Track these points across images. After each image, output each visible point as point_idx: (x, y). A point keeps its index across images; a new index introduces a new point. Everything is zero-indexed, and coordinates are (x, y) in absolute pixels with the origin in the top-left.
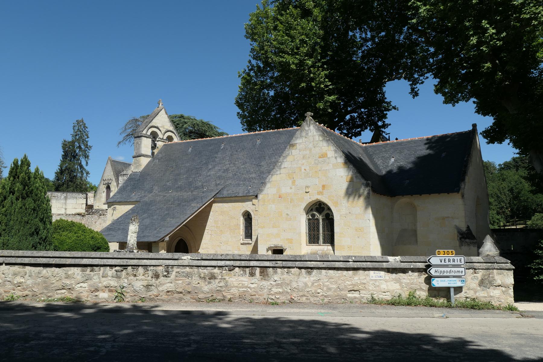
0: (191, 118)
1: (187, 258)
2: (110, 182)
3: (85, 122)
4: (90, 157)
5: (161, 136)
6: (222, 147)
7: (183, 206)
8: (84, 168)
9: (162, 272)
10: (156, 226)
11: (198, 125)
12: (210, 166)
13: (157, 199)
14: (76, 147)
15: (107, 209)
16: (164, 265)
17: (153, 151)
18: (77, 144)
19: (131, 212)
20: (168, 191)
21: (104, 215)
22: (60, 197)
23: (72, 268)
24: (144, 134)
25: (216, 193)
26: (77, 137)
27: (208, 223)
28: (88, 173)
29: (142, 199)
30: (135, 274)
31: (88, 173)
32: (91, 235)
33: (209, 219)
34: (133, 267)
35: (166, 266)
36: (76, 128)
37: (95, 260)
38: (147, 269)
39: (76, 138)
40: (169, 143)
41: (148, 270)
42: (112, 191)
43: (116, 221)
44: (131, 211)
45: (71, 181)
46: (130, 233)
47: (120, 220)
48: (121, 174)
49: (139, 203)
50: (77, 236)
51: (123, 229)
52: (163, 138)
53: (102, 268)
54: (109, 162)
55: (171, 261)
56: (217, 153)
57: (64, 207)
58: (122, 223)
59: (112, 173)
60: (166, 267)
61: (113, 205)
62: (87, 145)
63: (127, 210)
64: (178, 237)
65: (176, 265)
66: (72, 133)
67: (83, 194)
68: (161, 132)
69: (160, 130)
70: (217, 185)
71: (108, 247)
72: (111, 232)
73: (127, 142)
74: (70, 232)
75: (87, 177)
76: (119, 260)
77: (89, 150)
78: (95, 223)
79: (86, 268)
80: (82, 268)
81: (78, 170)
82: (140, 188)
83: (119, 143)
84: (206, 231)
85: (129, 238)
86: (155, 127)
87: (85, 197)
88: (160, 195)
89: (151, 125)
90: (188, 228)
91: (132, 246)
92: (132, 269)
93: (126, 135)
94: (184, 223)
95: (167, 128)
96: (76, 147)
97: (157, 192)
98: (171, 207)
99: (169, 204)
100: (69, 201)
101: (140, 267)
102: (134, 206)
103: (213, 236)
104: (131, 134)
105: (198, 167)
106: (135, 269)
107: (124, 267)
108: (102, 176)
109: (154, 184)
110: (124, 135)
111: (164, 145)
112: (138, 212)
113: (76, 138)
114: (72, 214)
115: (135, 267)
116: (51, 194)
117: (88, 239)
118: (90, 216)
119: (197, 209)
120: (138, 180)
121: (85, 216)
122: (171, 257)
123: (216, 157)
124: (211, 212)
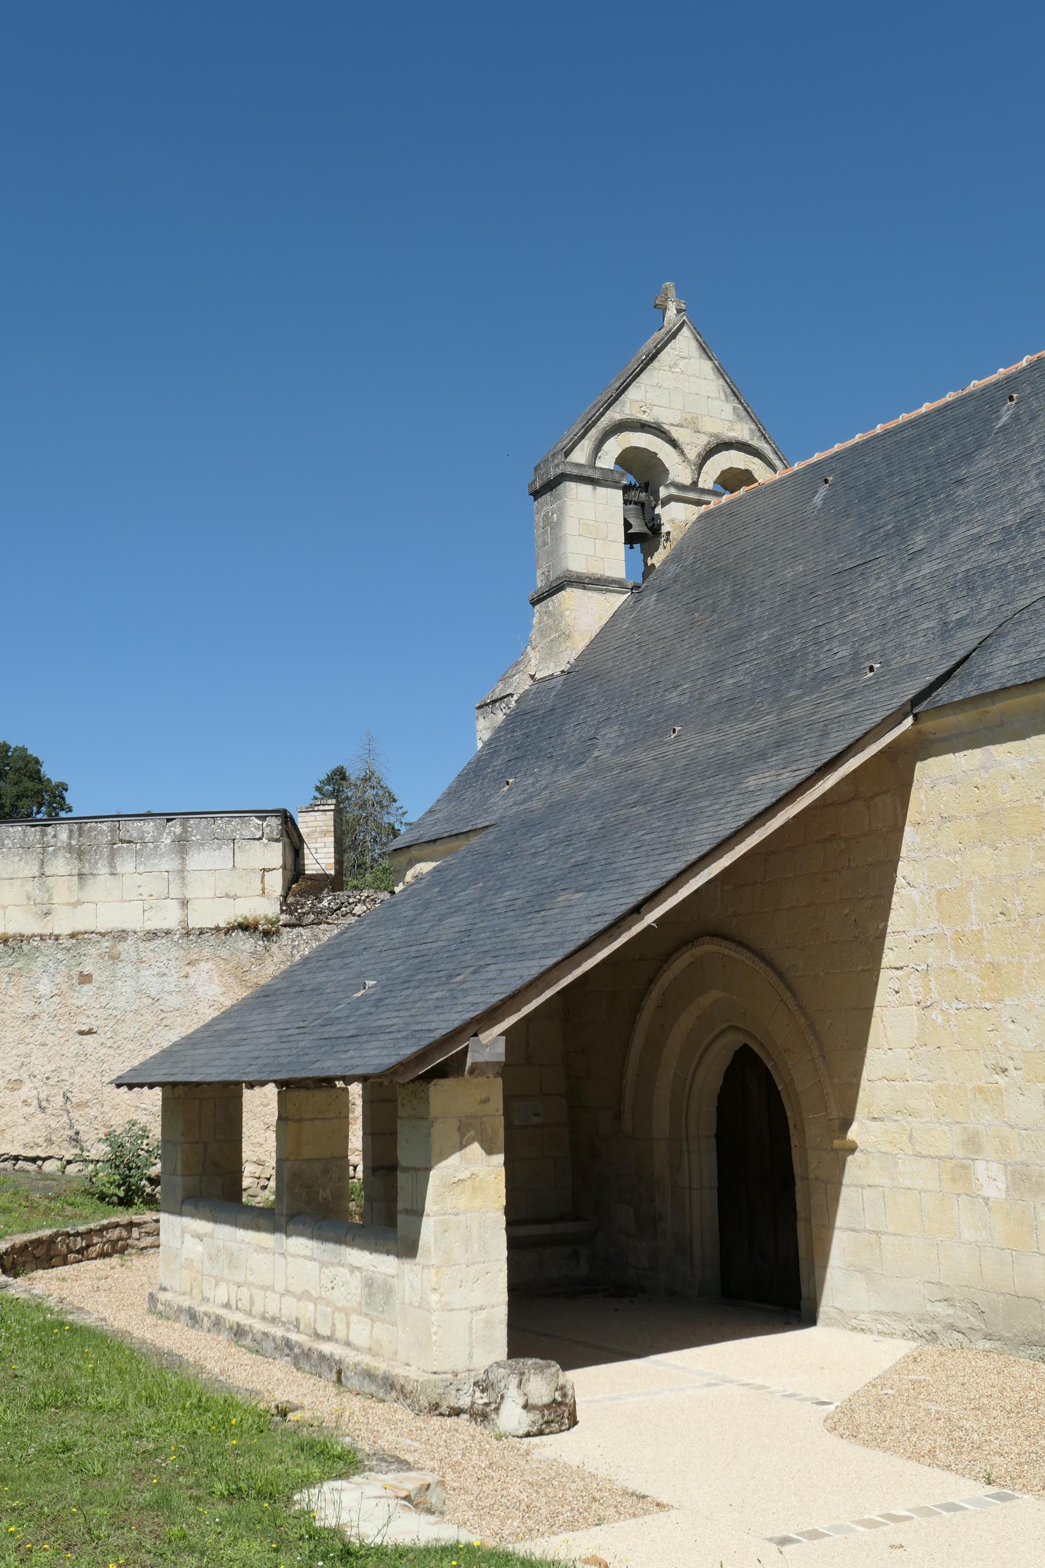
5: (679, 471)
22: (156, 840)
24: (579, 466)
27: (897, 919)
33: (900, 881)
52: (695, 483)
56: (968, 457)
57: (175, 891)
64: (723, 1032)
68: (682, 453)
69: (674, 443)
70: (945, 631)
84: (886, 980)
86: (643, 427)
89: (615, 414)
90: (770, 964)
94: (651, 918)
95: (715, 431)
100: (198, 860)
103: (935, 1014)
111: (701, 518)
114: (218, 929)
116: (112, 831)
121: (277, 932)
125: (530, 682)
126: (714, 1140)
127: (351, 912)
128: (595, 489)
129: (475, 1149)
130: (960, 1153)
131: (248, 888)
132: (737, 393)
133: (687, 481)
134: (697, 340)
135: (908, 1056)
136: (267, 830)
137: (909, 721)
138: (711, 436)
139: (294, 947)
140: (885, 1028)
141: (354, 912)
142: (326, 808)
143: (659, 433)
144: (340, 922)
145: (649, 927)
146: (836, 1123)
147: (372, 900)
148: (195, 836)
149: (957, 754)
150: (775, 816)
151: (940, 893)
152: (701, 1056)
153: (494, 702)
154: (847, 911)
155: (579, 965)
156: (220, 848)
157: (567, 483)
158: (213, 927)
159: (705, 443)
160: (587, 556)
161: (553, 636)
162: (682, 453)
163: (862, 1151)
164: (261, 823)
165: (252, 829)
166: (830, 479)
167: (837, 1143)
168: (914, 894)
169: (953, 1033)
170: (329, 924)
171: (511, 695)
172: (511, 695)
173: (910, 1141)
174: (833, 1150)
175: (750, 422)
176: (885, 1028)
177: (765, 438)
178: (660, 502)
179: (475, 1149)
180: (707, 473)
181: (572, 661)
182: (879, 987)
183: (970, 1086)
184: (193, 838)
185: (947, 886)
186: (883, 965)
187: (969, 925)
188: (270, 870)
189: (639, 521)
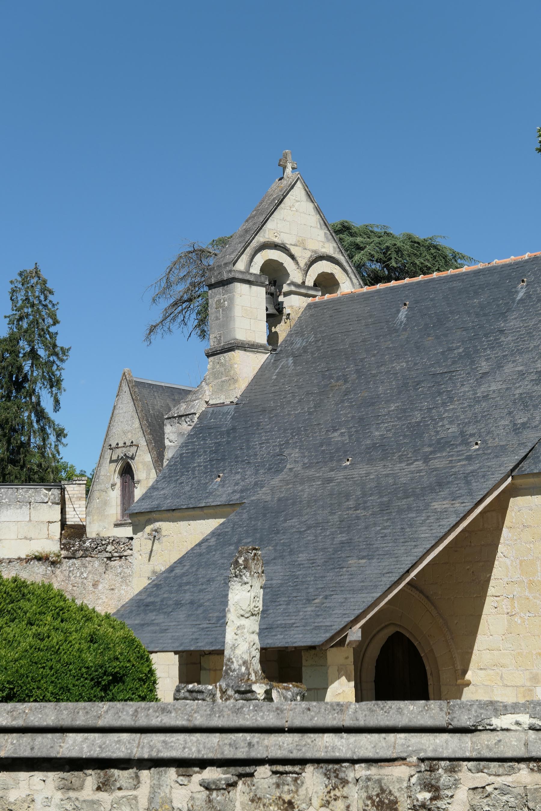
0: (376, 230)
1: (518, 723)
2: (130, 454)
3: (44, 274)
4: (64, 384)
5: (295, 275)
6: (521, 295)
7: (400, 511)
8: (48, 419)
9: (409, 787)
10: (311, 590)
11: (399, 251)
12: (484, 364)
13: (302, 491)
14: (21, 355)
15: (131, 535)
16: (414, 759)
17: (273, 330)
18: (24, 346)
19: (213, 541)
20: (340, 460)
21: (121, 557)
23: (23, 775)
24: (241, 272)
25: (518, 458)
26: (25, 324)
27: (497, 572)
28: (60, 434)
29: (249, 497)
30: (287, 798)
31: (60, 434)
32: (86, 631)
33: (499, 554)
34: (280, 768)
35: (422, 760)
36: (21, 296)
37: (114, 737)
38: (342, 775)
39: (20, 328)
40: (327, 297)
41: (345, 782)
42: (139, 482)
43: (166, 578)
44: (213, 539)
45: (14, 462)
46: (232, 617)
47: (178, 571)
48: (170, 415)
49: (238, 509)
50: (37, 636)
51: (192, 603)
52: (304, 283)
53: (145, 774)
54: (125, 388)
55: (445, 736)
56: (503, 315)
58: (188, 583)
59: (137, 424)
60: (423, 767)
61: (150, 522)
62: (55, 346)
63: (198, 539)
64: (386, 626)
65: (468, 755)
66: (10, 312)
67: (49, 490)
68: (297, 263)
69: (292, 257)
70: (517, 429)
71: (151, 672)
72: (152, 616)
73: (174, 327)
74: (12, 620)
75: (60, 447)
76: (215, 738)
77: (62, 361)
78: (95, 585)
79: (81, 773)
80: (61, 774)
81: (33, 426)
82: (237, 457)
83: (151, 331)
85: (230, 637)
87: (57, 500)
88: (311, 479)
89: (260, 239)
90: (421, 592)
91: (243, 669)
92: (275, 779)
93: (172, 301)
95: (314, 248)
96: (21, 355)
97: (298, 468)
98: (358, 518)
99: (349, 509)
101: (309, 768)
102: (222, 521)
103: (517, 619)
104: (186, 297)
105: (439, 370)
106: (289, 778)
107: (241, 770)
108: (109, 427)
109: (287, 443)
110: (165, 303)
111: (309, 306)
112: (239, 542)
113: (20, 328)
114: (19, 559)
115: (288, 768)
117: (77, 646)
118: (77, 562)
119: (453, 520)
120: (228, 433)
121: (60, 562)
122: (441, 721)
123: (502, 331)
124: (505, 530)
125: (205, 405)
126: (373, 684)
127: (105, 550)
128: (250, 287)
129: (344, 679)
130: (528, 684)
131: (39, 533)
132: (327, 224)
133: (299, 281)
134: (305, 190)
135: (501, 638)
136: (52, 497)
137: (510, 479)
138: (313, 252)
139: (70, 571)
140: (488, 625)
141: (107, 550)
142: (81, 482)
143: (284, 250)
144: (99, 556)
145: (412, 578)
146: (460, 672)
147: (117, 543)
148: (5, 499)
149: (533, 497)
150: (459, 526)
151: (521, 562)
152: (371, 639)
153: (180, 417)
154: (469, 567)
155: (387, 596)
156: (21, 508)
157: (236, 283)
158: (17, 558)
159: (309, 256)
160: (246, 330)
161: (223, 379)
162: (297, 263)
163: (473, 685)
164: (47, 492)
165: (42, 496)
166: (407, 303)
167: (459, 681)
168: (508, 561)
169: (526, 628)
170: (92, 557)
171: (195, 414)
172: (195, 414)
173: (501, 679)
174: (456, 685)
175: (333, 242)
176: (488, 625)
177: (342, 252)
178: (282, 293)
179: (344, 679)
180: (310, 276)
181: (238, 396)
182: (485, 605)
183: (534, 652)
184: (3, 501)
185: (525, 558)
186: (488, 594)
187: (536, 577)
188: (53, 522)
189: (271, 306)
